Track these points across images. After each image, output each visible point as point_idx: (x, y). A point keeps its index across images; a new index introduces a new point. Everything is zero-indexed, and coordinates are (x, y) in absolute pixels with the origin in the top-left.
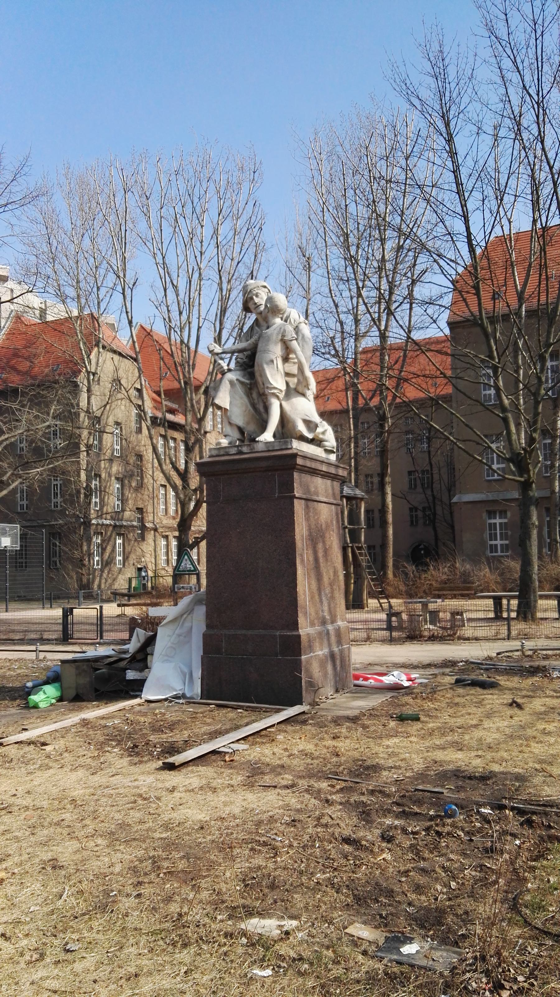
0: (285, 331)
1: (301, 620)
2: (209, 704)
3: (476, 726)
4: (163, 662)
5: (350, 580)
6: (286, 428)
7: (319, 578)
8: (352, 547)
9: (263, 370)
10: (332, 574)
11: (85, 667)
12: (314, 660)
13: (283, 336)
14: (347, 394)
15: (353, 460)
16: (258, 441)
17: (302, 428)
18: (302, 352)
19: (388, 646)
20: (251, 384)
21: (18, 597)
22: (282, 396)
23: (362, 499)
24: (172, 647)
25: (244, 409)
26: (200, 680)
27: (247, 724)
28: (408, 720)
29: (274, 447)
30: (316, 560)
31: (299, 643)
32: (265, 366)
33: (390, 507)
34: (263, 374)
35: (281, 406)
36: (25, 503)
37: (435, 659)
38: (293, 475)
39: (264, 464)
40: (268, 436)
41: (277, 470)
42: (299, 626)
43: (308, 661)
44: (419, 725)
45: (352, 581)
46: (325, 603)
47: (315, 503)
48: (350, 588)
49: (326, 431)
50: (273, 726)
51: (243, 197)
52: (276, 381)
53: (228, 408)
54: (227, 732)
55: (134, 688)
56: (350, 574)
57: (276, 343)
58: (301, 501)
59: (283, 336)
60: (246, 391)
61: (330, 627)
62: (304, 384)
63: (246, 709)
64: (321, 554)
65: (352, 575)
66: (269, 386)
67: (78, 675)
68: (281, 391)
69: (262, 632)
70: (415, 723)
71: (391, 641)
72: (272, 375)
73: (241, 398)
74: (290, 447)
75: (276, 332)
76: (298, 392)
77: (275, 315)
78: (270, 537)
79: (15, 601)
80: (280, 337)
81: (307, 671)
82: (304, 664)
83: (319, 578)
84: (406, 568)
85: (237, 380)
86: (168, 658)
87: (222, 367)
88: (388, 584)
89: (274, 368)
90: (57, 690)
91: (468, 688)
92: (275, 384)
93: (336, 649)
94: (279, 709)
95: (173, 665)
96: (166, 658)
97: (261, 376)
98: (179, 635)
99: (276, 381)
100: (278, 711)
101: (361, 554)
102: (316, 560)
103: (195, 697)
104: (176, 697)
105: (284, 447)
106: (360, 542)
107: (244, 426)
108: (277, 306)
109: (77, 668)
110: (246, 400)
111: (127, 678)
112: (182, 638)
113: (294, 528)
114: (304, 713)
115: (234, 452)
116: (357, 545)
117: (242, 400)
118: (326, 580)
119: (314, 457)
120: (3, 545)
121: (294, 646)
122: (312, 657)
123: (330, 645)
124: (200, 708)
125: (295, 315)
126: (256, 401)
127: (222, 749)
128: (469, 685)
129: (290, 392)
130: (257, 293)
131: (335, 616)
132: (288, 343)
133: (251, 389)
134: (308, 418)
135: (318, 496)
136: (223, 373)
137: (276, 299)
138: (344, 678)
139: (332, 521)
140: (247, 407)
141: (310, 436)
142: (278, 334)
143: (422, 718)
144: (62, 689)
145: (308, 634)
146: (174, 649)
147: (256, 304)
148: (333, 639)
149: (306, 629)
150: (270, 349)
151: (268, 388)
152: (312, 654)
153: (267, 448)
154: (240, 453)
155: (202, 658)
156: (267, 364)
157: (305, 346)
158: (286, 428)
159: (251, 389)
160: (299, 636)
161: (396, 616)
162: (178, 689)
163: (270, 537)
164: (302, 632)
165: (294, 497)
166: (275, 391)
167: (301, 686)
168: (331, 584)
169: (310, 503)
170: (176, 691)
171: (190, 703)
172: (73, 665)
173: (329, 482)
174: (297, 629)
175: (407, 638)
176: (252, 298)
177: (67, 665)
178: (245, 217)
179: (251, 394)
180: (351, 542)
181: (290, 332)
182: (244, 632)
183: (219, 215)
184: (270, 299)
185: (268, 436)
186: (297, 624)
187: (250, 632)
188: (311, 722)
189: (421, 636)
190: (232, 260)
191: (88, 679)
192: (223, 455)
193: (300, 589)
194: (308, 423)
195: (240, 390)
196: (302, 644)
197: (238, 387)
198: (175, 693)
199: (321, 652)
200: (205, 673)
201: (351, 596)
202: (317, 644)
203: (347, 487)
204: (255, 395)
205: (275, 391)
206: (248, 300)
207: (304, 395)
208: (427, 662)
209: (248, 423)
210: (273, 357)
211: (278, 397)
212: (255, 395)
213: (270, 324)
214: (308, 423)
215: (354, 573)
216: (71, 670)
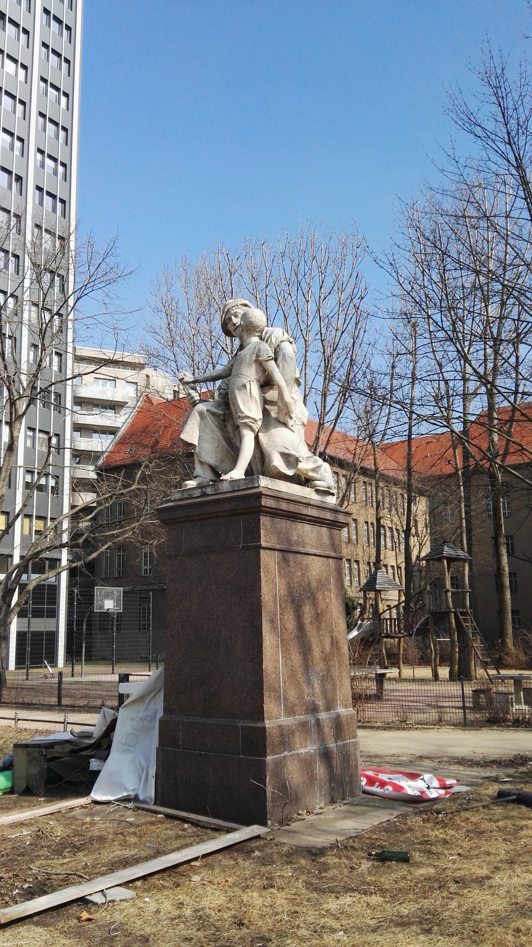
0: (259, 350)
1: (270, 706)
2: (157, 813)
3: (481, 881)
4: (123, 752)
5: (455, 650)
6: (261, 464)
7: (306, 651)
8: (455, 613)
9: (235, 397)
10: (328, 646)
11: (36, 754)
12: (293, 761)
13: (258, 356)
14: (455, 452)
15: (464, 521)
16: (223, 480)
17: (278, 463)
18: (282, 374)
19: (461, 732)
20: (224, 415)
21: (141, 658)
22: (257, 426)
23: (465, 560)
24: (133, 734)
25: (216, 444)
26: (154, 780)
27: (178, 849)
28: (391, 860)
29: (239, 486)
30: (300, 627)
31: (264, 738)
32: (237, 392)
33: (507, 569)
34: (236, 404)
35: (257, 438)
36: (148, 567)
37: (503, 752)
38: (259, 520)
39: (226, 507)
40: (238, 473)
41: (241, 514)
42: (266, 715)
43: (279, 764)
44: (402, 870)
45: (457, 650)
46: (317, 684)
47: (306, 556)
48: (455, 658)
49: (319, 467)
50: (196, 859)
51: (346, 273)
52: (249, 409)
53: (196, 443)
54: (147, 859)
55: (84, 783)
56: (455, 641)
57: (250, 365)
58: (272, 552)
59: (258, 356)
60: (219, 423)
61: (323, 716)
62: (285, 411)
63: (195, 824)
64: (307, 619)
65: (457, 643)
66: (241, 415)
67: (30, 762)
68: (255, 420)
69: (222, 721)
70: (400, 865)
71: (465, 725)
72: (244, 402)
73: (213, 432)
74: (256, 485)
75: (250, 352)
76: (280, 422)
77: (251, 334)
78: (233, 598)
79: (137, 662)
80: (254, 358)
81: (278, 775)
82: (270, 767)
83: (306, 651)
84: (526, 635)
85: (207, 411)
86: (129, 747)
87: (193, 398)
88: (507, 654)
89: (246, 394)
90: (7, 780)
91: (510, 806)
92: (247, 413)
93: (332, 745)
94: (231, 828)
95: (129, 757)
96: (126, 747)
97: (234, 404)
98: (143, 719)
99: (249, 409)
100: (229, 831)
101: (465, 620)
102: (300, 627)
103: (148, 800)
104: (126, 800)
105: (250, 486)
106: (464, 606)
107: (217, 464)
108: (251, 323)
109: (29, 754)
110: (218, 433)
111: (91, 769)
112: (145, 722)
113: (260, 587)
114: (258, 837)
115: (198, 495)
116: (461, 610)
117: (214, 433)
118: (316, 652)
119: (292, 498)
120: (106, 607)
121: (256, 742)
122: (285, 757)
123: (322, 740)
124: (146, 816)
125: (278, 333)
126: (231, 435)
127: (92, 898)
128: (513, 801)
129: (268, 420)
130: (236, 313)
131: (334, 701)
132: (264, 363)
133: (224, 421)
134: (287, 451)
135: (304, 547)
136: (194, 404)
137: (250, 315)
138: (342, 782)
139: (327, 579)
140: (219, 442)
141: (290, 472)
142: (252, 355)
143: (417, 856)
144: (14, 779)
145: (280, 726)
146: (137, 736)
147: (234, 324)
148: (328, 731)
149: (276, 718)
150: (243, 373)
151: (239, 417)
152: (286, 753)
153: (232, 487)
154: (204, 495)
155: (158, 751)
156: (239, 389)
157: (286, 366)
158: (261, 464)
159: (224, 421)
160: (264, 728)
161: (484, 693)
162: (130, 789)
163: (233, 598)
164: (268, 724)
165: (260, 547)
166: (247, 421)
167: (265, 798)
168: (326, 659)
169: (291, 557)
170: (126, 790)
171: (139, 808)
172: (24, 750)
173: (324, 530)
174: (262, 719)
175: (487, 722)
176: (230, 319)
177: (19, 750)
178: (348, 291)
179: (226, 427)
180: (454, 607)
181: (267, 351)
182: (203, 720)
183: (321, 288)
184: (245, 316)
185: (238, 473)
186: (262, 712)
187: (209, 721)
188: (257, 853)
189: (505, 720)
190: (337, 330)
191: (38, 769)
192: (187, 499)
193: (267, 664)
194: (287, 457)
195: (211, 422)
196: (268, 740)
197: (209, 419)
198: (125, 794)
199: (308, 748)
200: (160, 772)
201: (457, 667)
202: (297, 739)
203: (448, 547)
204: (229, 428)
205: (247, 421)
206: (227, 321)
207: (285, 425)
208: (494, 757)
209: (222, 461)
210: (245, 381)
211: (252, 430)
212: (229, 428)
213: (244, 344)
214: (287, 457)
215: (458, 641)
216: (21, 758)
